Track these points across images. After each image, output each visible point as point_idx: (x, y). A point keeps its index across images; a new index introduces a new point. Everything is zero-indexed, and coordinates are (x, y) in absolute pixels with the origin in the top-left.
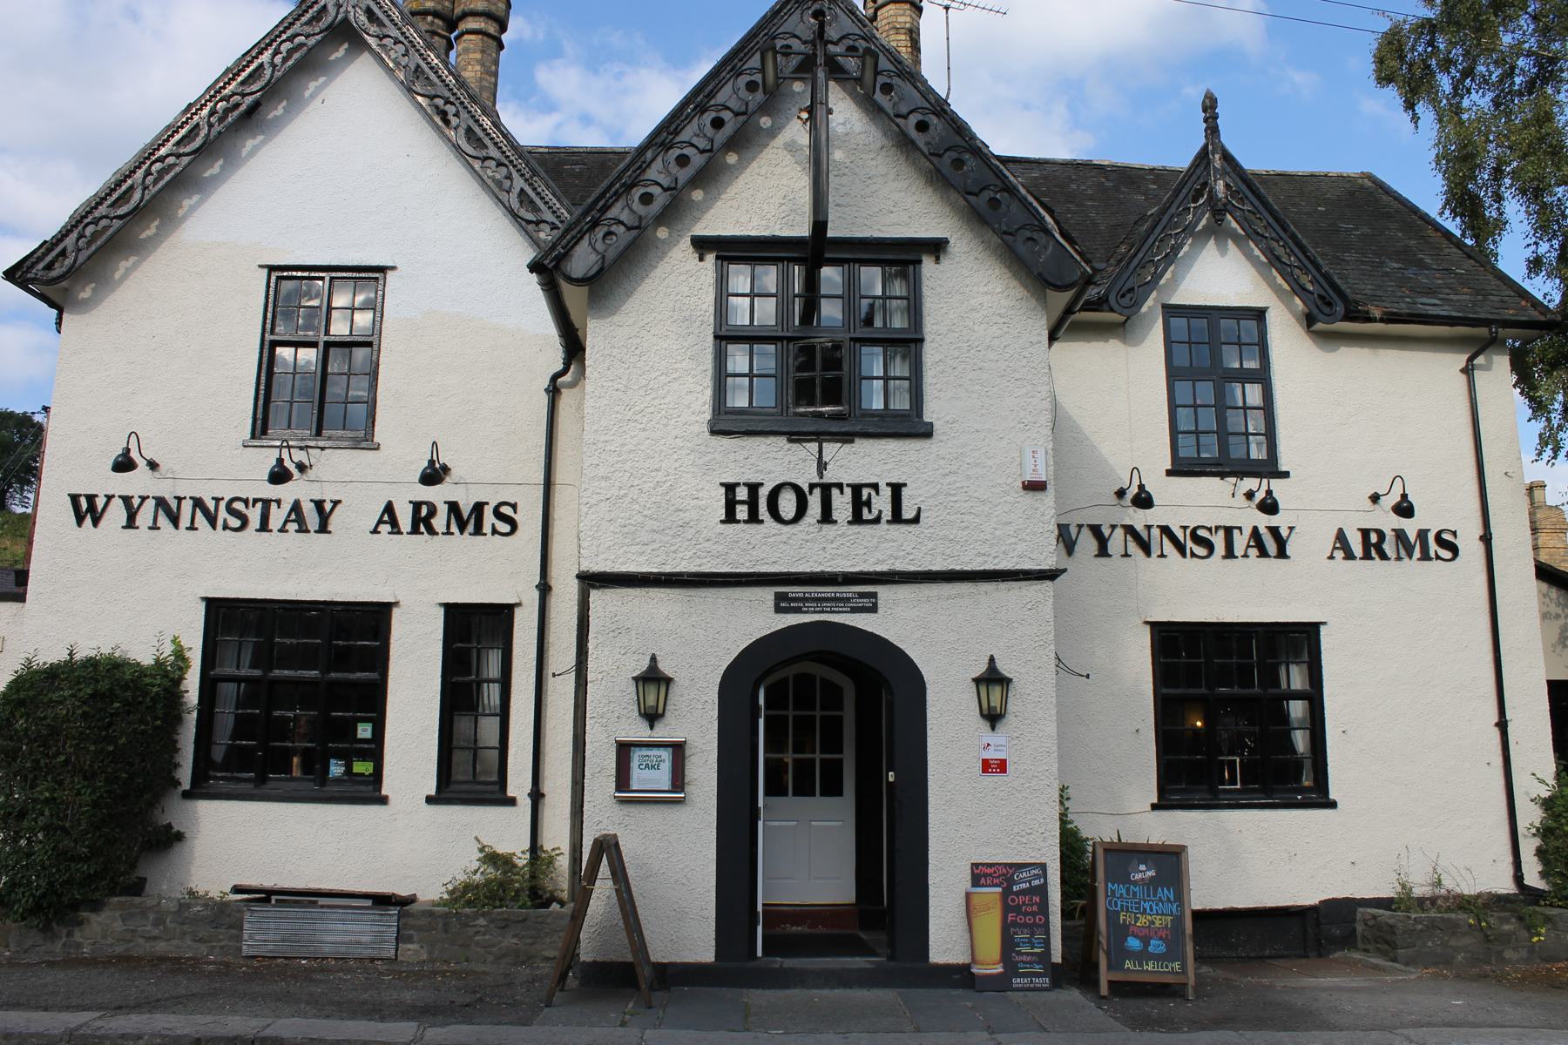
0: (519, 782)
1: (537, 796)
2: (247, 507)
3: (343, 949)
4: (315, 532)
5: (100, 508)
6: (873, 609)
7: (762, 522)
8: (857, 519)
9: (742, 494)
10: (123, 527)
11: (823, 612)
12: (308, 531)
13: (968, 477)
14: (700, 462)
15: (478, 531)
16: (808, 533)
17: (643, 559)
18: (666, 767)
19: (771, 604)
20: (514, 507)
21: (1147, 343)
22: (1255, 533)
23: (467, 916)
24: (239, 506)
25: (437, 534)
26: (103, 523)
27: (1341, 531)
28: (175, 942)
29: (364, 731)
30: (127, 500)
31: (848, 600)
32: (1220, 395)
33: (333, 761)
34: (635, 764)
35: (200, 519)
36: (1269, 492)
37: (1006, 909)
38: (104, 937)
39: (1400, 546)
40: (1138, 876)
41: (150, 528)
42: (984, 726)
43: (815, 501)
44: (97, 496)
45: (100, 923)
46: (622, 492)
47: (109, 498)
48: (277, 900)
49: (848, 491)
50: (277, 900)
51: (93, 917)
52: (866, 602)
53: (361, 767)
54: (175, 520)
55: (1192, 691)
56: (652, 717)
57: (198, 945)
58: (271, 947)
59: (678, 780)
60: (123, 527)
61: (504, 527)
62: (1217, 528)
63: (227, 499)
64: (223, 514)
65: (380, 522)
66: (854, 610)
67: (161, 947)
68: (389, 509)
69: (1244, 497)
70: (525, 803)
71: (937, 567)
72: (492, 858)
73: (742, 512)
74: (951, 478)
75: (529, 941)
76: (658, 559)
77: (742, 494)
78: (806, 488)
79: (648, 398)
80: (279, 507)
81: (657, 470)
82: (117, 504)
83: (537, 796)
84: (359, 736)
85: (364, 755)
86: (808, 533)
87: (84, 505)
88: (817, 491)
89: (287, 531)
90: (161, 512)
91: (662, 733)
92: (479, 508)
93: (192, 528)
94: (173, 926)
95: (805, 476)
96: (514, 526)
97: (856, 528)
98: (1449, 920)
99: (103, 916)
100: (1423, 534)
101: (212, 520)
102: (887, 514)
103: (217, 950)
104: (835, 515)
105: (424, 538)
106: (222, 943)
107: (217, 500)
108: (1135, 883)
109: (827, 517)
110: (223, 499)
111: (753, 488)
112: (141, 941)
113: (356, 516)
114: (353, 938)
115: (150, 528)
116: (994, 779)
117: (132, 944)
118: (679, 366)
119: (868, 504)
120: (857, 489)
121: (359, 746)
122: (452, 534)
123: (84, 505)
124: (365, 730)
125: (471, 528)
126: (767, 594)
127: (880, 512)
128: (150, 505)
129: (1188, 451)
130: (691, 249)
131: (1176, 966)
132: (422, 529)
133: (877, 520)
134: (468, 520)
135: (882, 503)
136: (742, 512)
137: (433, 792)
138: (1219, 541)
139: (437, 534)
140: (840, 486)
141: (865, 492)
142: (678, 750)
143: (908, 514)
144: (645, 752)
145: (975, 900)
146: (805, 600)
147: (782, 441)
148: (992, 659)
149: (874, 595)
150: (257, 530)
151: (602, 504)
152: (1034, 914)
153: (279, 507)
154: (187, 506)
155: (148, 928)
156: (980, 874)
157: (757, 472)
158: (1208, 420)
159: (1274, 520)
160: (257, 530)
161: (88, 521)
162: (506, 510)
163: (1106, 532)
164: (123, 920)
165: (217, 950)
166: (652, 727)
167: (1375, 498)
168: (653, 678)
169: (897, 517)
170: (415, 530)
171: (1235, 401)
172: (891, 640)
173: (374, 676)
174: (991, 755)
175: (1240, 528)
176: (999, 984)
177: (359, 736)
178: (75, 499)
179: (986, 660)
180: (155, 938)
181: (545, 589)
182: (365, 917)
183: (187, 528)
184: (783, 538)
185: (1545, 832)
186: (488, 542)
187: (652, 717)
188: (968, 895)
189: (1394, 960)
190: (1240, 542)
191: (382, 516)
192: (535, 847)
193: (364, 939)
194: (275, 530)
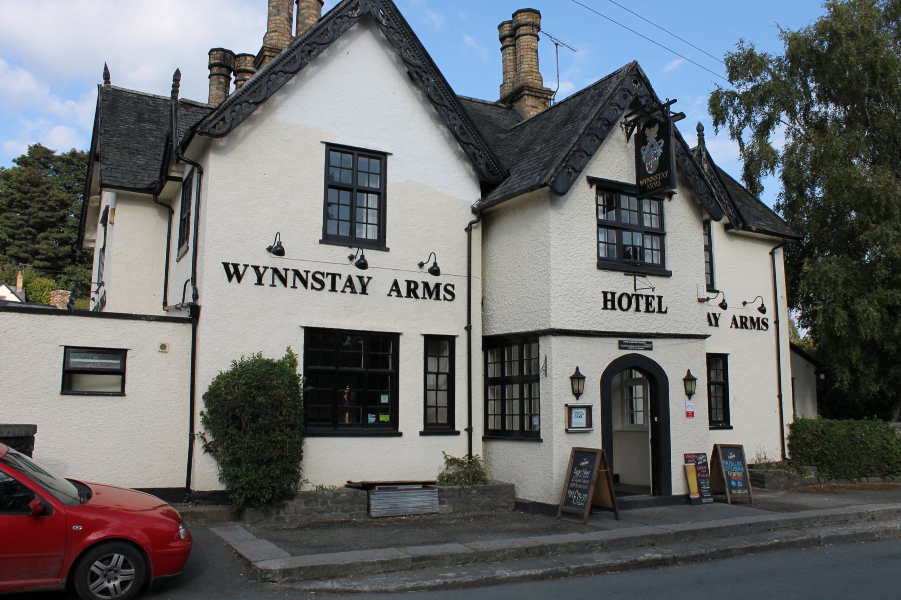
0: (460, 423)
1: (469, 430)
2: (324, 277)
3: (417, 510)
4: (360, 293)
5: (241, 273)
6: (651, 349)
7: (616, 309)
8: (647, 311)
10: (256, 284)
11: (635, 349)
12: (356, 293)
13: (681, 295)
14: (594, 281)
15: (438, 298)
16: (632, 315)
17: (575, 324)
18: (584, 416)
19: (617, 345)
20: (453, 286)
22: (350, 279)
23: (468, 489)
24: (319, 276)
25: (419, 298)
26: (243, 281)
27: (350, 276)
28: (333, 513)
29: (385, 399)
30: (256, 268)
31: (642, 345)
32: (353, 201)
33: (369, 415)
34: (573, 416)
35: (298, 282)
36: (362, 257)
37: (698, 472)
38: (296, 513)
39: (426, 292)
40: (731, 457)
41: (270, 286)
42: (686, 398)
43: (634, 300)
44: (239, 264)
45: (294, 506)
46: (567, 293)
47: (246, 266)
48: (379, 488)
49: (644, 298)
50: (379, 488)
51: (289, 503)
52: (648, 346)
53: (384, 418)
54: (284, 281)
55: (324, 368)
56: (577, 394)
57: (345, 513)
58: (385, 512)
59: (589, 423)
60: (256, 284)
61: (449, 297)
62: (328, 274)
63: (312, 272)
64: (310, 280)
65: (392, 290)
66: (645, 349)
67: (326, 516)
68: (396, 283)
69: (267, 251)
70: (464, 435)
71: (672, 332)
72: (451, 462)
73: (609, 305)
74: (676, 295)
75: (494, 499)
76: (580, 324)
77: (609, 297)
79: (575, 250)
80: (340, 279)
81: (579, 284)
82: (251, 272)
83: (469, 430)
84: (382, 402)
85: (385, 412)
86: (632, 315)
87: (232, 270)
88: (634, 297)
89: (345, 292)
90: (276, 276)
91: (582, 401)
93: (294, 287)
94: (331, 505)
95: (631, 291)
97: (647, 314)
98: (779, 471)
99: (295, 502)
100: (438, 286)
101: (305, 283)
102: (657, 310)
103: (355, 515)
104: (641, 308)
106: (356, 512)
107: (307, 272)
108: (730, 460)
109: (638, 309)
110: (310, 272)
111: (613, 294)
112: (316, 514)
113: (380, 285)
114: (421, 504)
115: (270, 286)
116: (691, 419)
117: (311, 516)
118: (584, 236)
119: (651, 304)
120: (647, 297)
121: (382, 407)
122: (426, 298)
123: (232, 270)
124: (385, 399)
125: (434, 296)
126: (615, 341)
128: (269, 272)
129: (332, 231)
130: (586, 182)
131: (746, 491)
132: (412, 295)
133: (653, 311)
134: (433, 292)
135: (655, 304)
136: (609, 305)
137: (422, 430)
138: (328, 281)
139: (419, 298)
140: (642, 296)
141: (650, 299)
142: (589, 409)
143: (663, 310)
144: (577, 410)
145: (688, 469)
146: (629, 344)
147: (622, 274)
148: (689, 371)
149: (651, 343)
150: (329, 291)
151: (559, 298)
152: (705, 473)
153: (340, 279)
154: (290, 275)
155: (319, 507)
156: (688, 458)
157: (614, 287)
158: (345, 213)
159: (364, 273)
160: (329, 291)
161: (235, 278)
162: (449, 288)
163: (262, 270)
164: (306, 503)
165: (355, 515)
166: (577, 399)
167: (421, 265)
168: (577, 378)
169: (660, 311)
171: (363, 204)
172: (657, 362)
173: (310, 367)
174: (689, 410)
175: (340, 275)
176: (698, 501)
177: (382, 402)
178: (226, 265)
179: (686, 371)
180: (323, 512)
181: (468, 329)
182: (425, 494)
183: (292, 287)
184: (623, 317)
185: (791, 438)
186: (442, 303)
187: (577, 394)
188: (685, 467)
189: (764, 488)
190: (340, 283)
191: (392, 287)
192: (470, 455)
193: (426, 504)
194: (339, 291)
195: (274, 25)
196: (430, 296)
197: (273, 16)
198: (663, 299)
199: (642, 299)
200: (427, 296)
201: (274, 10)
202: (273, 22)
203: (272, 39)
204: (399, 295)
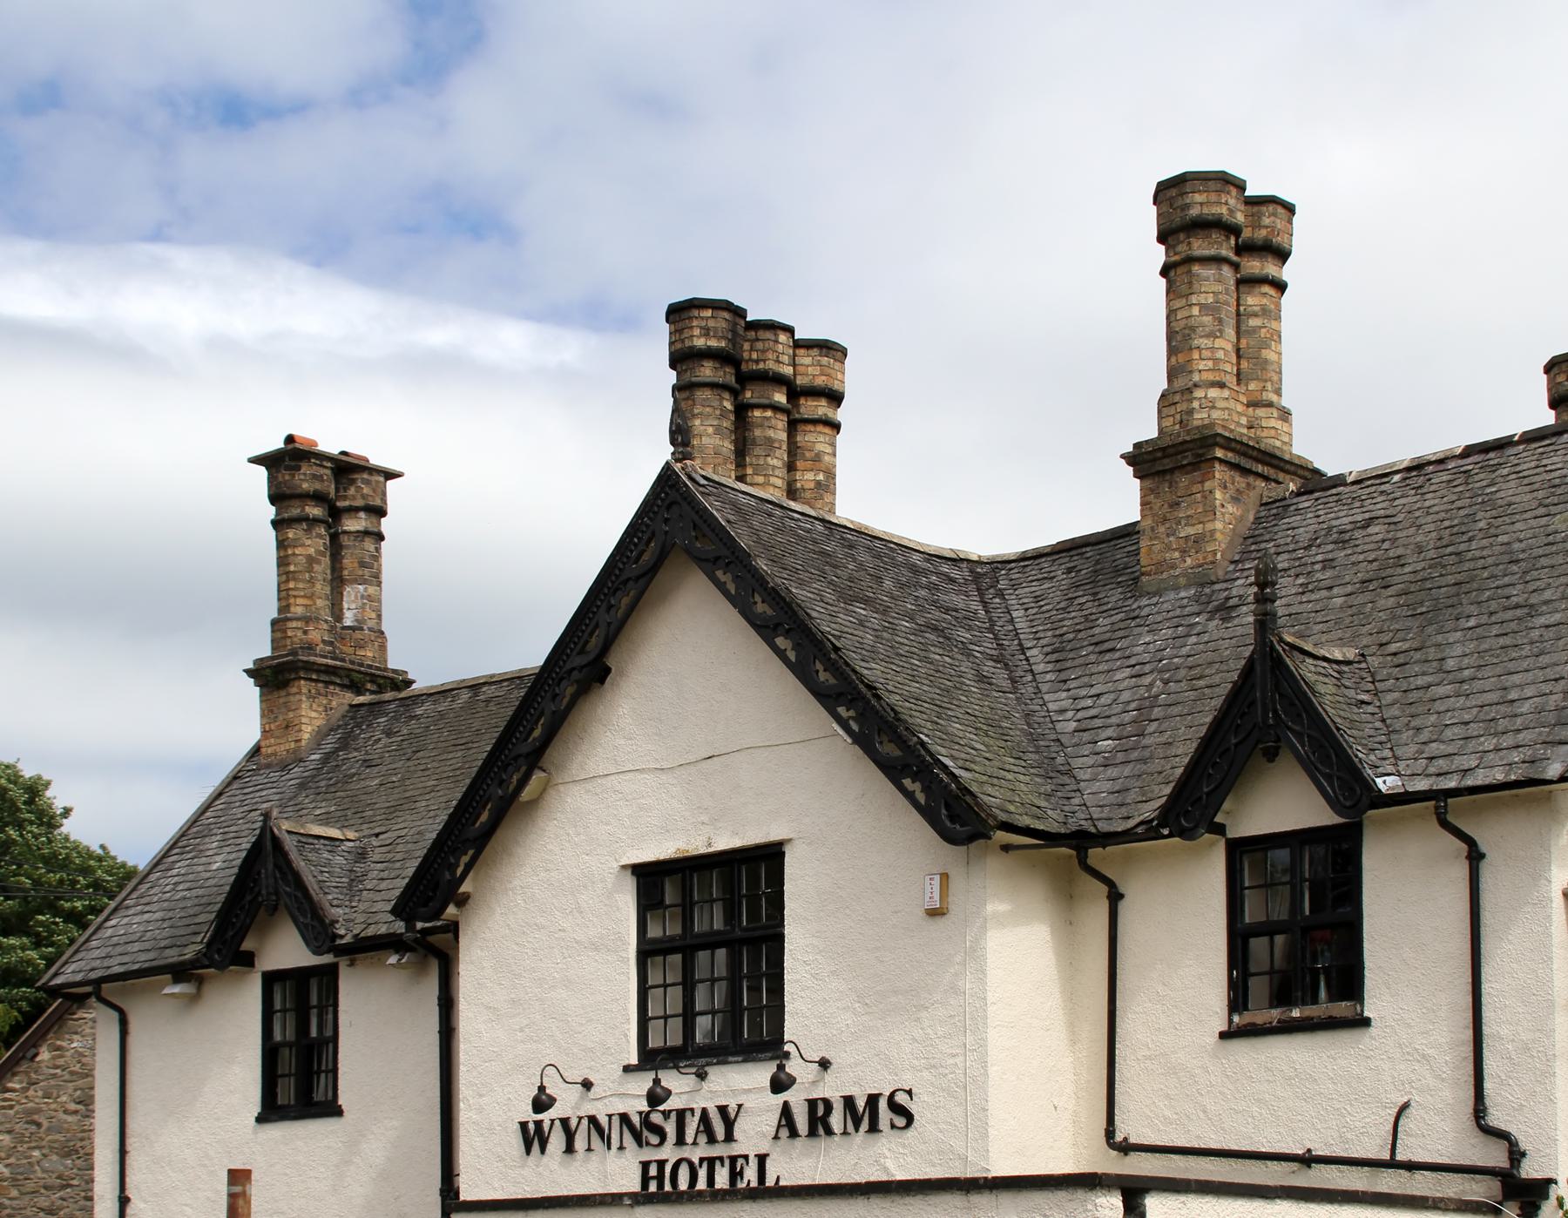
9: (653, 1171)
15: (874, 1128)
21: (1336, 817)
39: (867, 1111)
49: (727, 1162)
77: (653, 1171)
78: (696, 1161)
88: (705, 1165)
92: (873, 1100)
93: (621, 1148)
96: (910, 1118)
105: (823, 1142)
119: (741, 1174)
125: (865, 1125)
127: (749, 1181)
132: (821, 1131)
140: (721, 1159)
161: (536, 1147)
170: (812, 1133)
195: (1210, 364)
196: (857, 1125)
197: (1207, 336)
198: (768, 1162)
199: (723, 1165)
200: (850, 1128)
201: (1207, 319)
202: (1205, 354)
203: (1214, 407)
204: (794, 1134)
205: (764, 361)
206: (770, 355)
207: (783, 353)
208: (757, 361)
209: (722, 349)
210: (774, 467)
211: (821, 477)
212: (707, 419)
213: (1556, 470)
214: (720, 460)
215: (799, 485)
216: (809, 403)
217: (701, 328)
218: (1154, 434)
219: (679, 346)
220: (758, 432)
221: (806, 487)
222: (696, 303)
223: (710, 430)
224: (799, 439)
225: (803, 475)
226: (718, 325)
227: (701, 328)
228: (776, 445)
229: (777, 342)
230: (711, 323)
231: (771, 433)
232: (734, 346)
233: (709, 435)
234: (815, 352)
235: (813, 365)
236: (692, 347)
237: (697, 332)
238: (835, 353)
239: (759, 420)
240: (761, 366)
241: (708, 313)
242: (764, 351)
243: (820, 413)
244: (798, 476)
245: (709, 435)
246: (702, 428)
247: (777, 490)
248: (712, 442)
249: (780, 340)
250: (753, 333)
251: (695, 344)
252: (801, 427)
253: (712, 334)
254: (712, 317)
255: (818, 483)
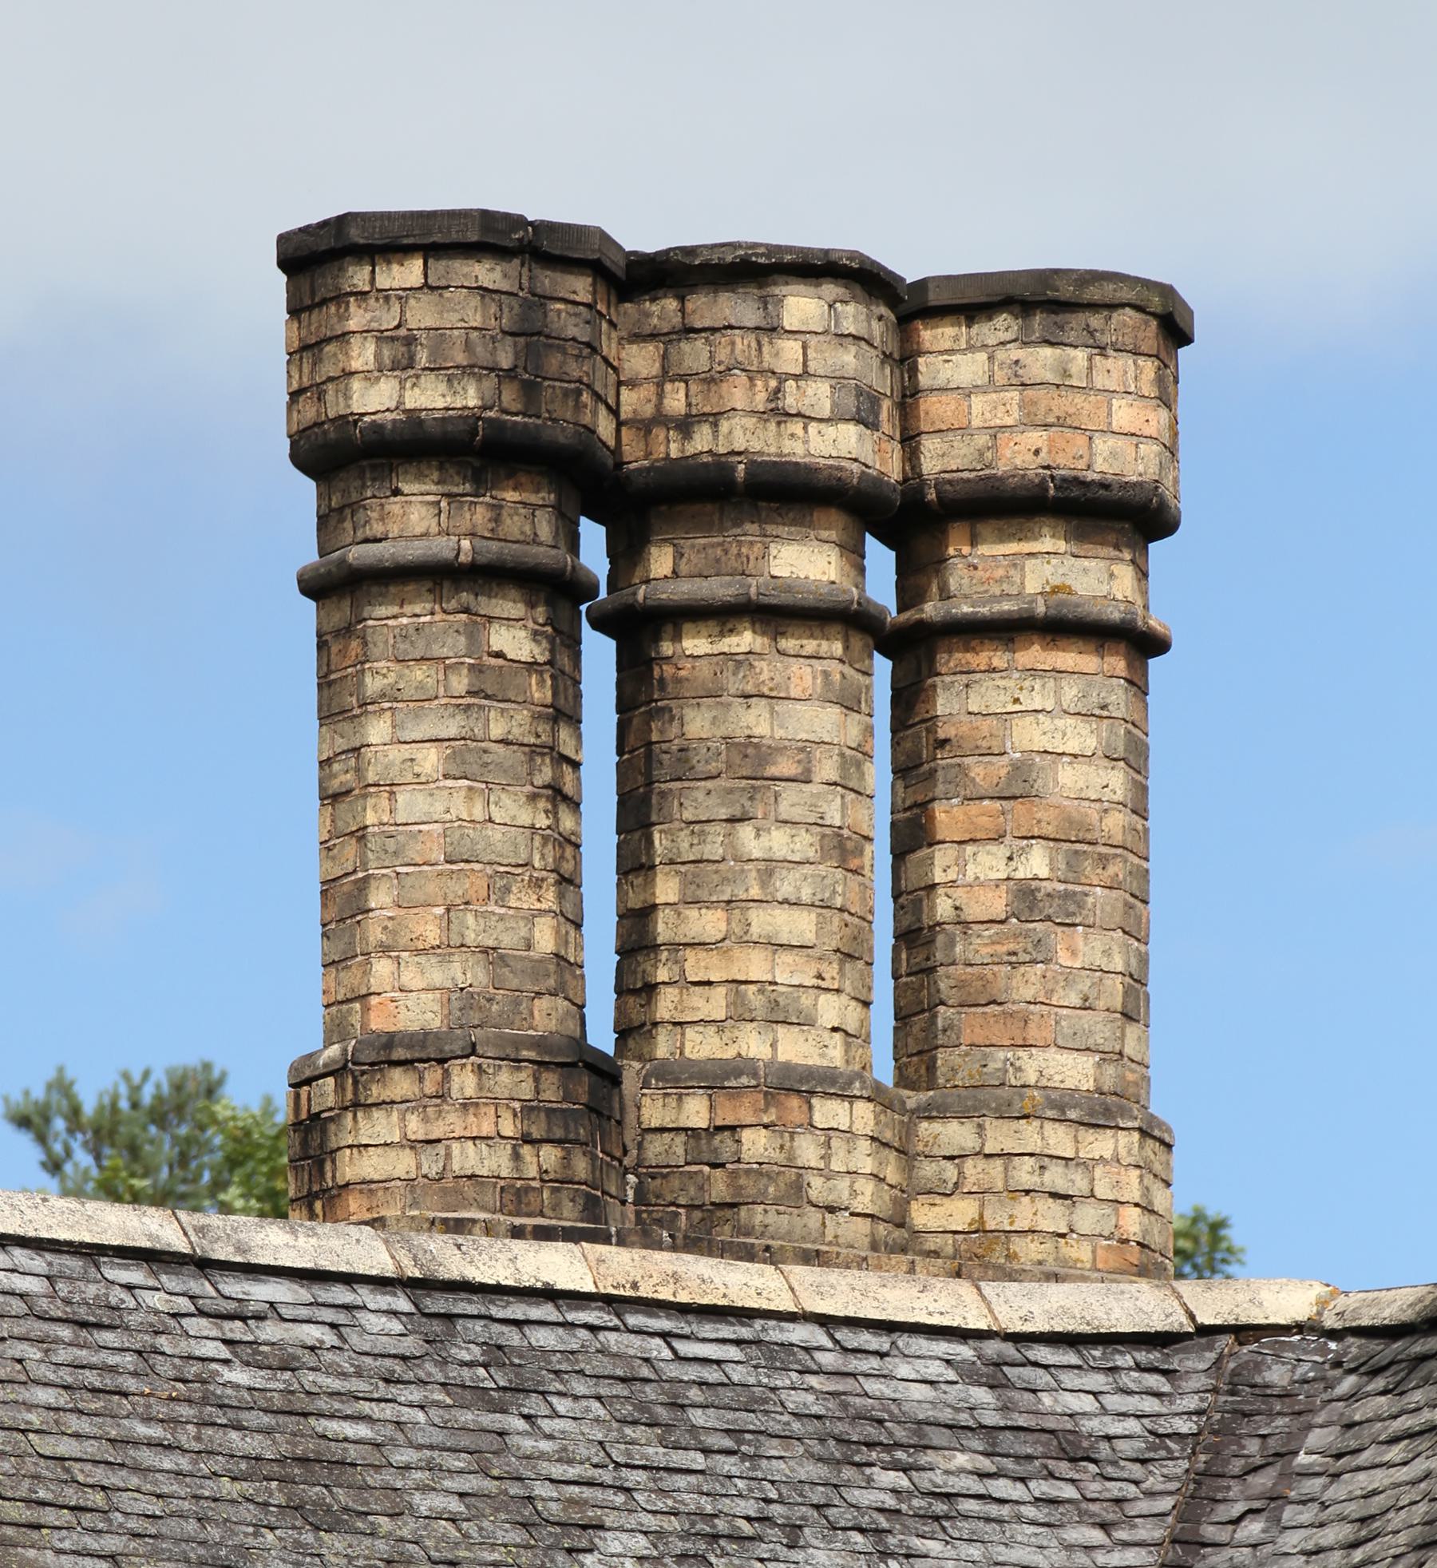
205: (714, 419)
206: (737, 393)
207: (805, 374)
208: (685, 425)
209: (470, 419)
210: (769, 867)
211: (1037, 863)
212: (417, 715)
213: (724, 1341)
214: (473, 883)
215: (943, 908)
216: (984, 549)
217: (383, 338)
218: (1151, 661)
219: (309, 412)
220: (698, 723)
221: (973, 912)
222: (356, 235)
223: (430, 759)
224: (943, 704)
225: (961, 864)
226: (451, 320)
227: (383, 338)
228: (785, 766)
229: (773, 330)
230: (422, 315)
231: (756, 721)
232: (530, 391)
233: (419, 781)
234: (1003, 326)
235: (990, 386)
236: (346, 421)
237: (363, 355)
238: (1096, 320)
239: (705, 670)
240: (702, 441)
241: (411, 272)
242: (711, 380)
243: (1032, 586)
244: (942, 864)
245: (419, 781)
246: (397, 754)
247: (786, 957)
248: (438, 809)
249: (789, 321)
250: (671, 304)
251: (357, 407)
252: (950, 660)
253: (423, 358)
254: (426, 286)
255: (1026, 896)
